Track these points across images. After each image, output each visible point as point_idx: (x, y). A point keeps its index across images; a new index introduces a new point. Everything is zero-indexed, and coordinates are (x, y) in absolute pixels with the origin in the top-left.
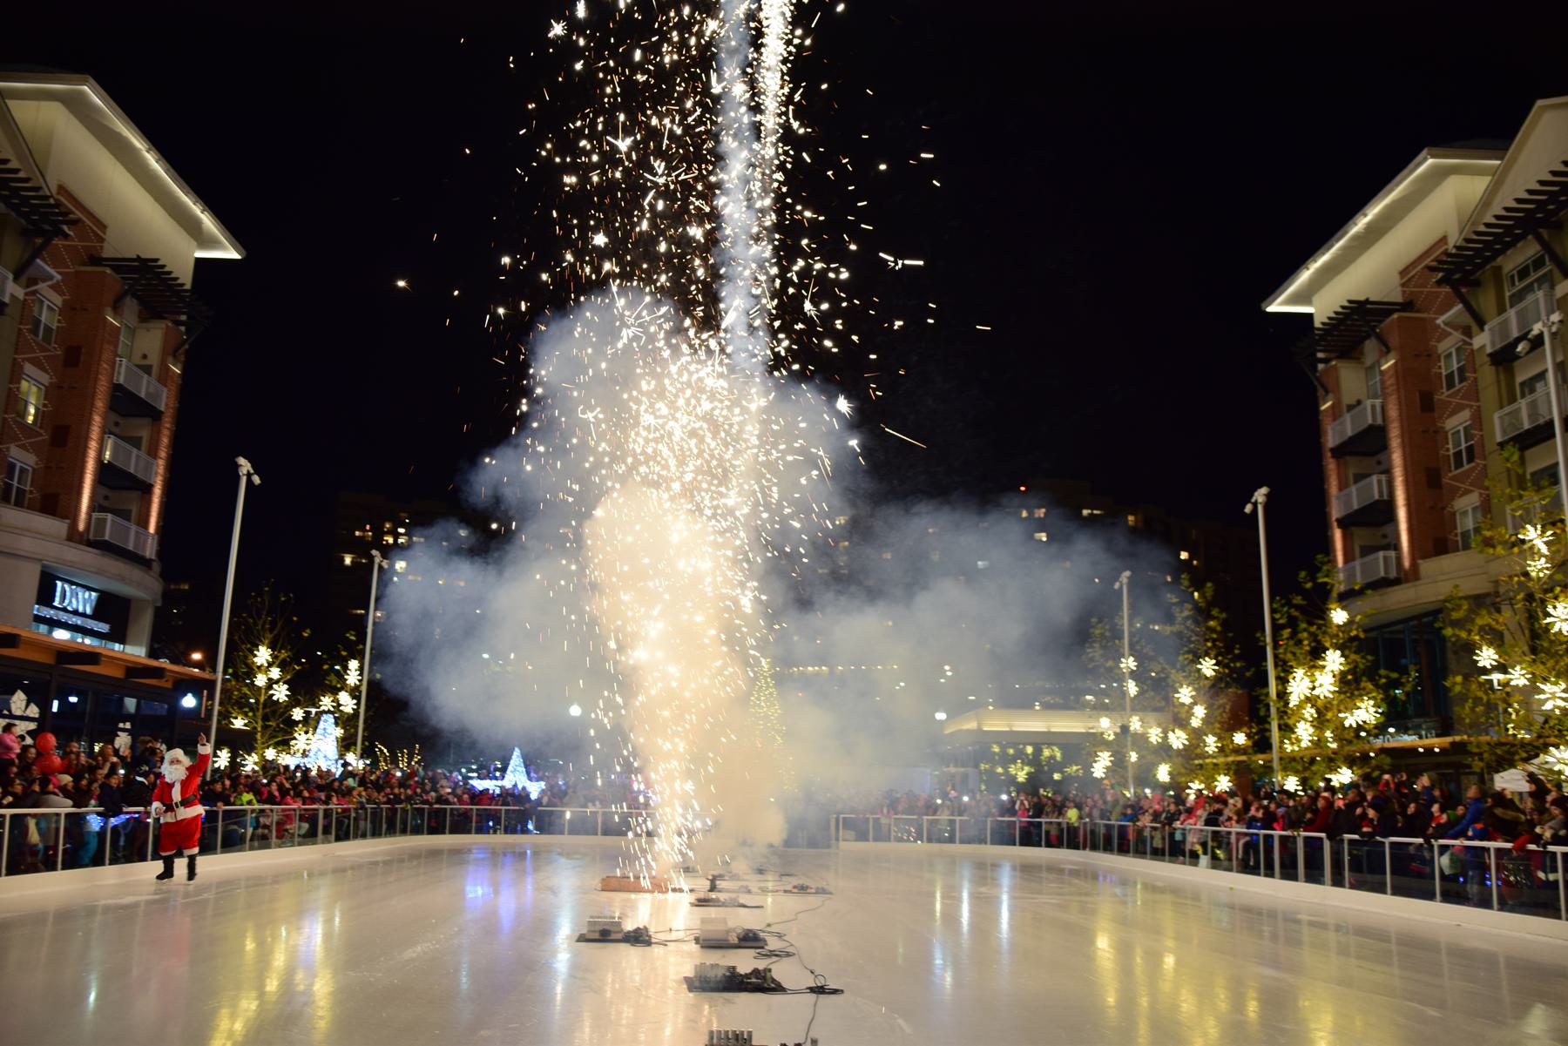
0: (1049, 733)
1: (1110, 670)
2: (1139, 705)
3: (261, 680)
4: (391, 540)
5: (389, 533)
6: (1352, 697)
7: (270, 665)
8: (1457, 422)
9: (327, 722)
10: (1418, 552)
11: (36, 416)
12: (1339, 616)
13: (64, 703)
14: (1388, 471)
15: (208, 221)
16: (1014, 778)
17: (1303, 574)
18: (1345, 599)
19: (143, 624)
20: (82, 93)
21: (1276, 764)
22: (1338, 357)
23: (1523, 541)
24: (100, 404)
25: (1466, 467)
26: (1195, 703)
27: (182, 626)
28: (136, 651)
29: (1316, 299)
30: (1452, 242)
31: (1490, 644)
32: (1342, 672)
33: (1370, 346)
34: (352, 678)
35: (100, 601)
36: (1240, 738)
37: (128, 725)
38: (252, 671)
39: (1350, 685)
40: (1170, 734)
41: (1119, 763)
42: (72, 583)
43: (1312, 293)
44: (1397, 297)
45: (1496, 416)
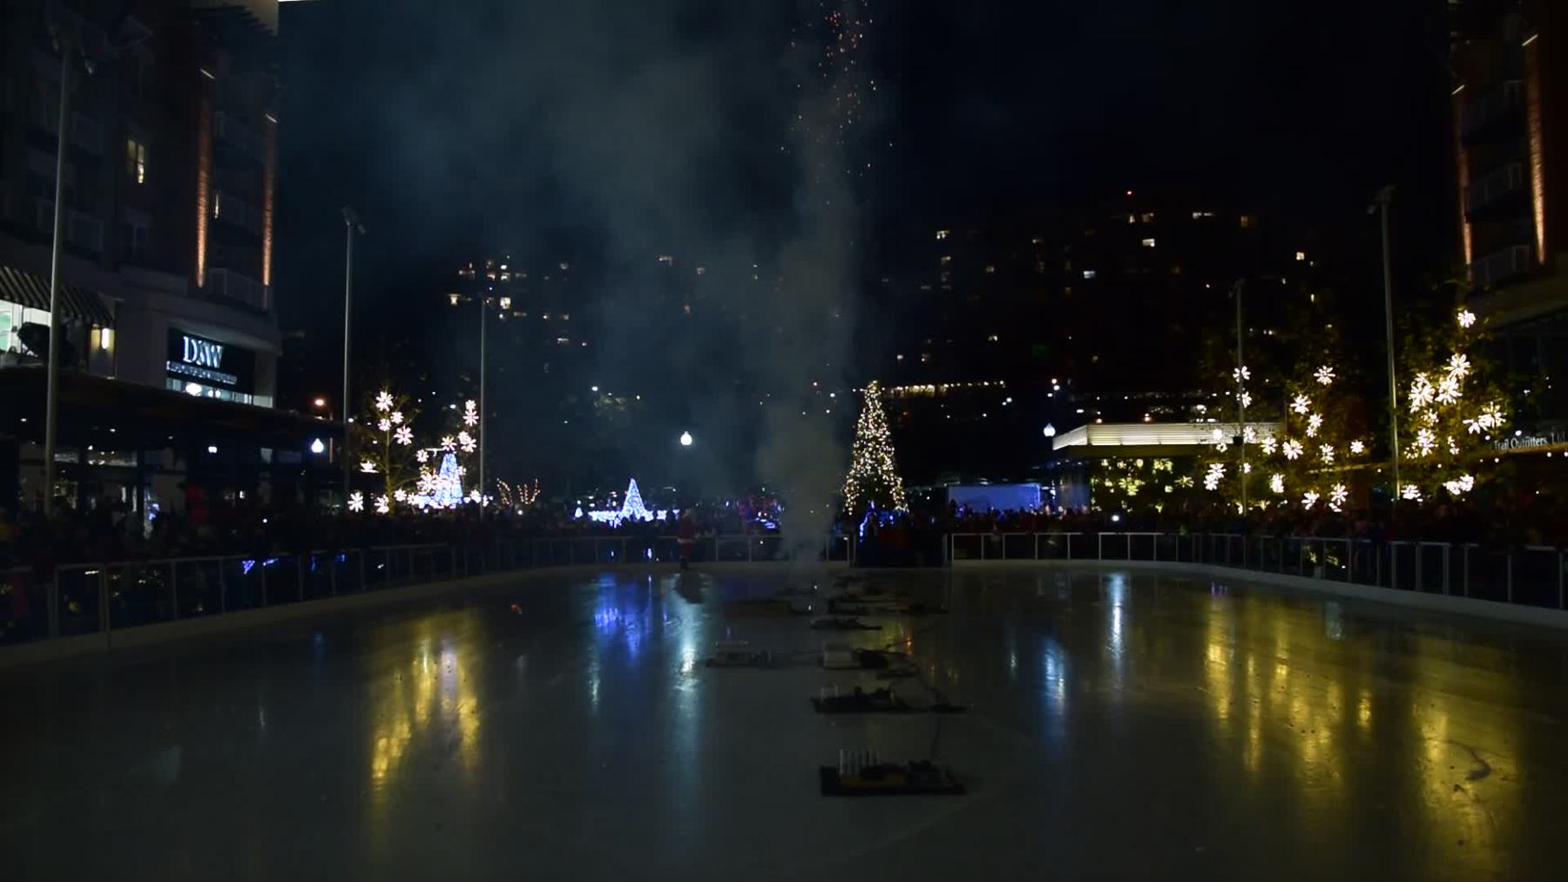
2: (1255, 415)
3: (385, 425)
5: (491, 271)
7: (392, 409)
9: (450, 462)
11: (145, 175)
12: (1466, 319)
16: (1125, 491)
26: (1311, 413)
27: (292, 391)
28: (265, 402)
34: (471, 418)
35: (224, 353)
36: (1357, 447)
38: (376, 416)
39: (1475, 393)
40: (1286, 445)
41: (1232, 473)
42: (197, 339)
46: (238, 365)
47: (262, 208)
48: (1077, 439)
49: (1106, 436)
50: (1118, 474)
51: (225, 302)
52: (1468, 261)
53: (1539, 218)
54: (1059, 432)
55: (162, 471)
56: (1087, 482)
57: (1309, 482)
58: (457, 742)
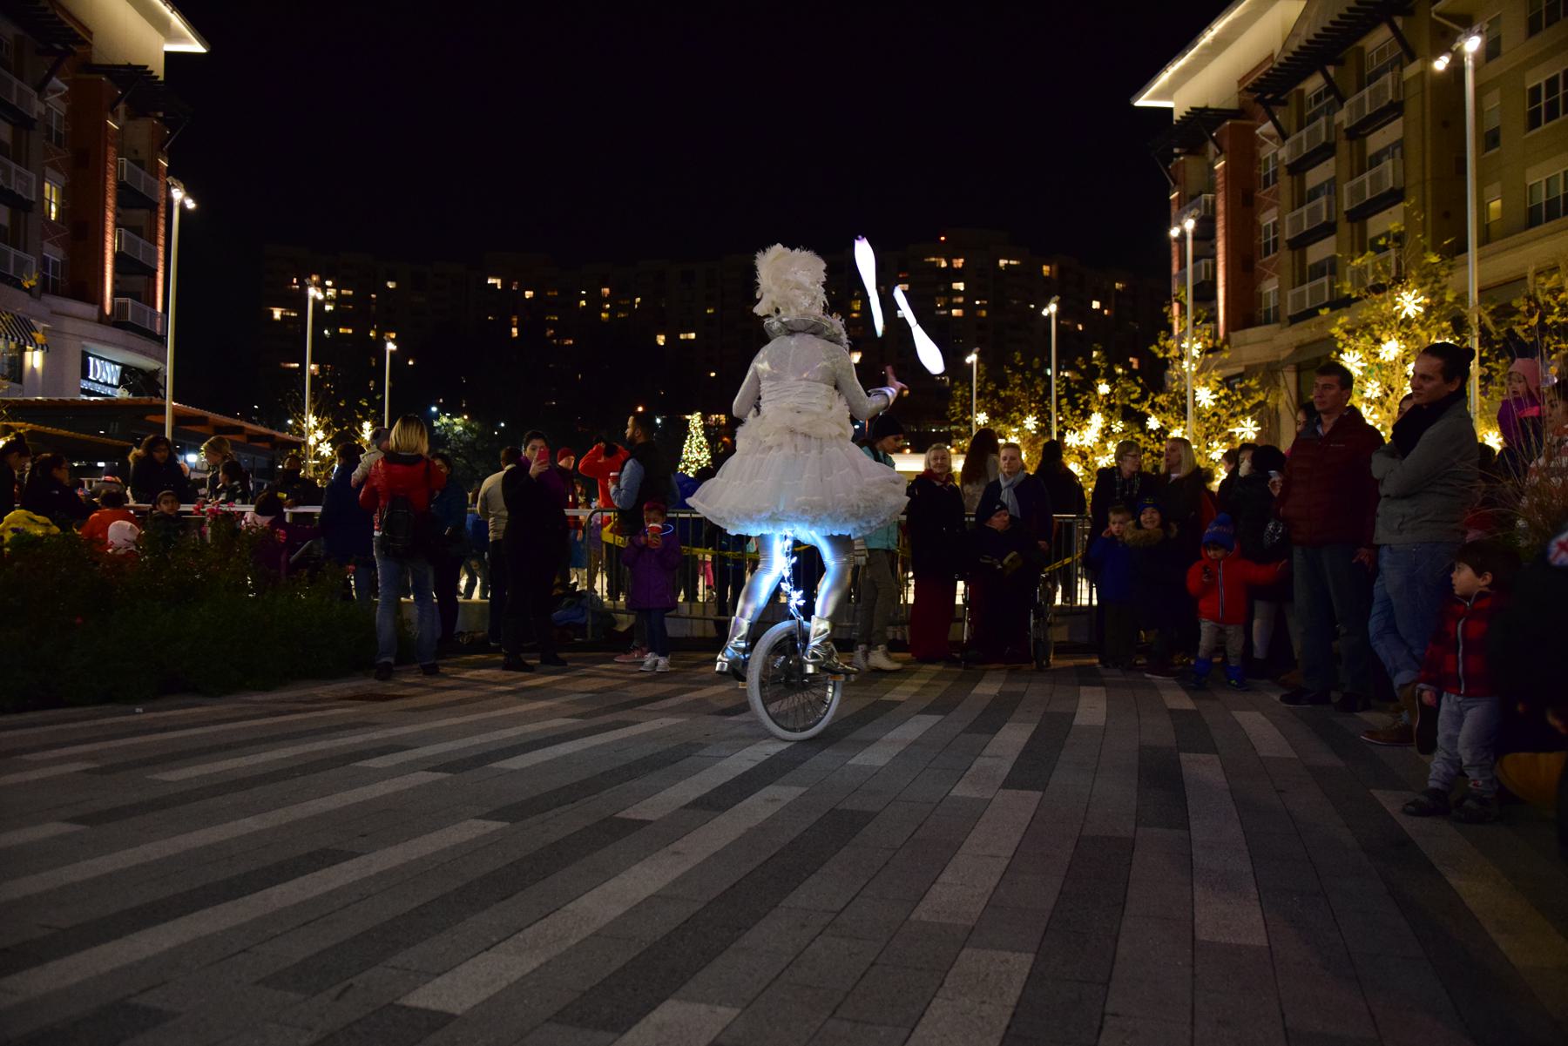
10: (1231, 325)
12: (1104, 389)
14: (1214, 257)
15: (176, 20)
24: (110, 201)
29: (1176, 95)
43: (1175, 90)
44: (1233, 105)
45: (1345, 187)
47: (156, 244)
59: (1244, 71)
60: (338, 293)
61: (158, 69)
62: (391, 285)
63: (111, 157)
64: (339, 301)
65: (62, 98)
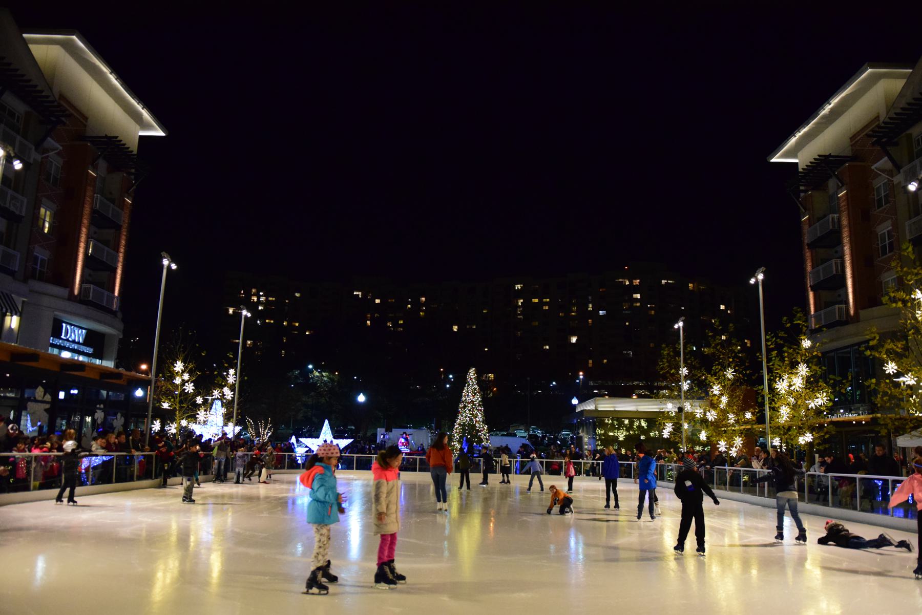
0: (637, 412)
1: (673, 375)
3: (178, 381)
4: (255, 299)
5: (254, 295)
6: (813, 391)
7: (183, 372)
8: (884, 228)
11: (49, 228)
12: (806, 344)
13: (68, 394)
15: (146, 114)
16: (617, 438)
17: (785, 318)
18: (812, 335)
19: (114, 349)
20: (72, 40)
21: (768, 431)
22: (812, 190)
23: (914, 299)
24: (85, 221)
25: (889, 255)
26: (722, 395)
27: (127, 358)
28: (109, 364)
29: (799, 154)
30: (882, 120)
31: (892, 360)
32: (807, 377)
33: (832, 183)
34: (231, 380)
35: (87, 334)
36: (748, 415)
37: (102, 406)
38: (173, 375)
39: (812, 384)
40: (708, 414)
41: (677, 428)
42: (71, 325)
43: (796, 151)
44: (848, 153)
45: (907, 224)
46: (94, 341)
47: (118, 251)
48: (589, 406)
49: (606, 405)
50: (613, 428)
51: (88, 303)
52: (812, 313)
53: (850, 290)
54: (581, 401)
55: (36, 401)
56: (594, 431)
57: (720, 434)
58: (206, 583)
59: (853, 131)
60: (267, 299)
61: (134, 146)
62: (297, 295)
63: (89, 193)
64: (267, 303)
65: (58, 154)
